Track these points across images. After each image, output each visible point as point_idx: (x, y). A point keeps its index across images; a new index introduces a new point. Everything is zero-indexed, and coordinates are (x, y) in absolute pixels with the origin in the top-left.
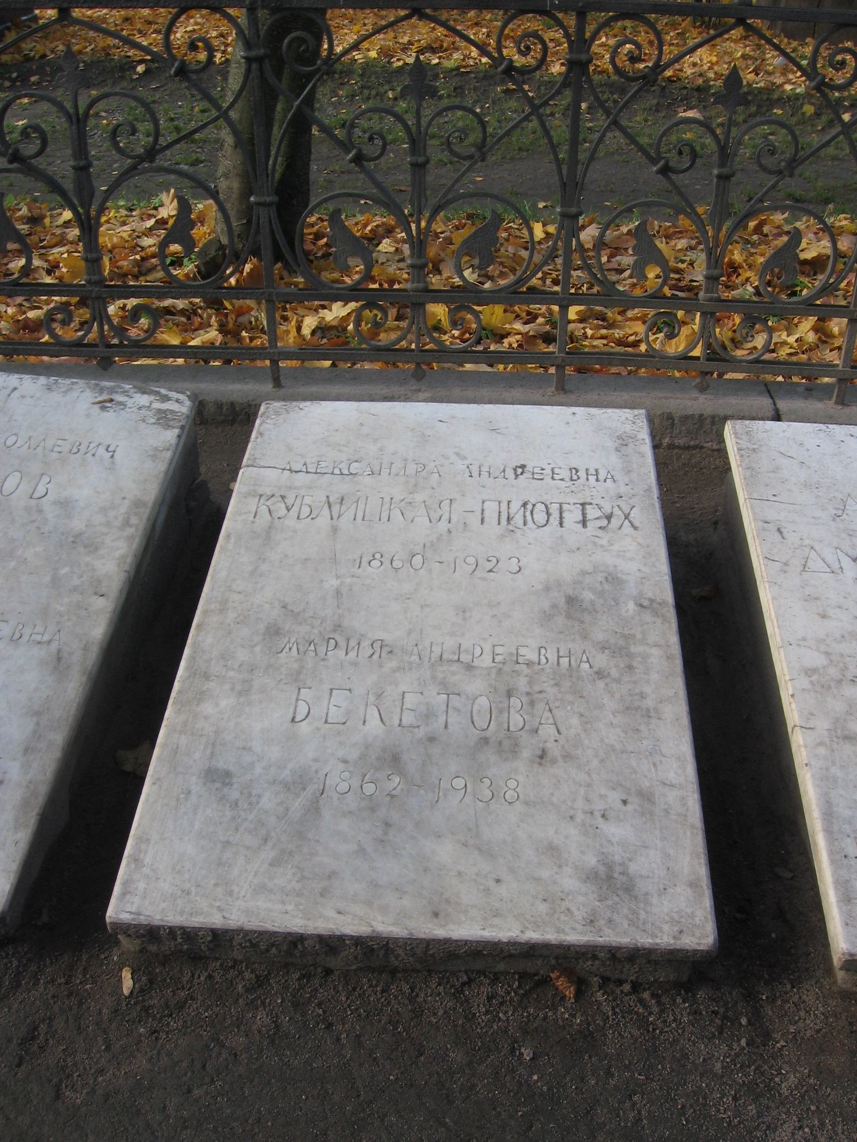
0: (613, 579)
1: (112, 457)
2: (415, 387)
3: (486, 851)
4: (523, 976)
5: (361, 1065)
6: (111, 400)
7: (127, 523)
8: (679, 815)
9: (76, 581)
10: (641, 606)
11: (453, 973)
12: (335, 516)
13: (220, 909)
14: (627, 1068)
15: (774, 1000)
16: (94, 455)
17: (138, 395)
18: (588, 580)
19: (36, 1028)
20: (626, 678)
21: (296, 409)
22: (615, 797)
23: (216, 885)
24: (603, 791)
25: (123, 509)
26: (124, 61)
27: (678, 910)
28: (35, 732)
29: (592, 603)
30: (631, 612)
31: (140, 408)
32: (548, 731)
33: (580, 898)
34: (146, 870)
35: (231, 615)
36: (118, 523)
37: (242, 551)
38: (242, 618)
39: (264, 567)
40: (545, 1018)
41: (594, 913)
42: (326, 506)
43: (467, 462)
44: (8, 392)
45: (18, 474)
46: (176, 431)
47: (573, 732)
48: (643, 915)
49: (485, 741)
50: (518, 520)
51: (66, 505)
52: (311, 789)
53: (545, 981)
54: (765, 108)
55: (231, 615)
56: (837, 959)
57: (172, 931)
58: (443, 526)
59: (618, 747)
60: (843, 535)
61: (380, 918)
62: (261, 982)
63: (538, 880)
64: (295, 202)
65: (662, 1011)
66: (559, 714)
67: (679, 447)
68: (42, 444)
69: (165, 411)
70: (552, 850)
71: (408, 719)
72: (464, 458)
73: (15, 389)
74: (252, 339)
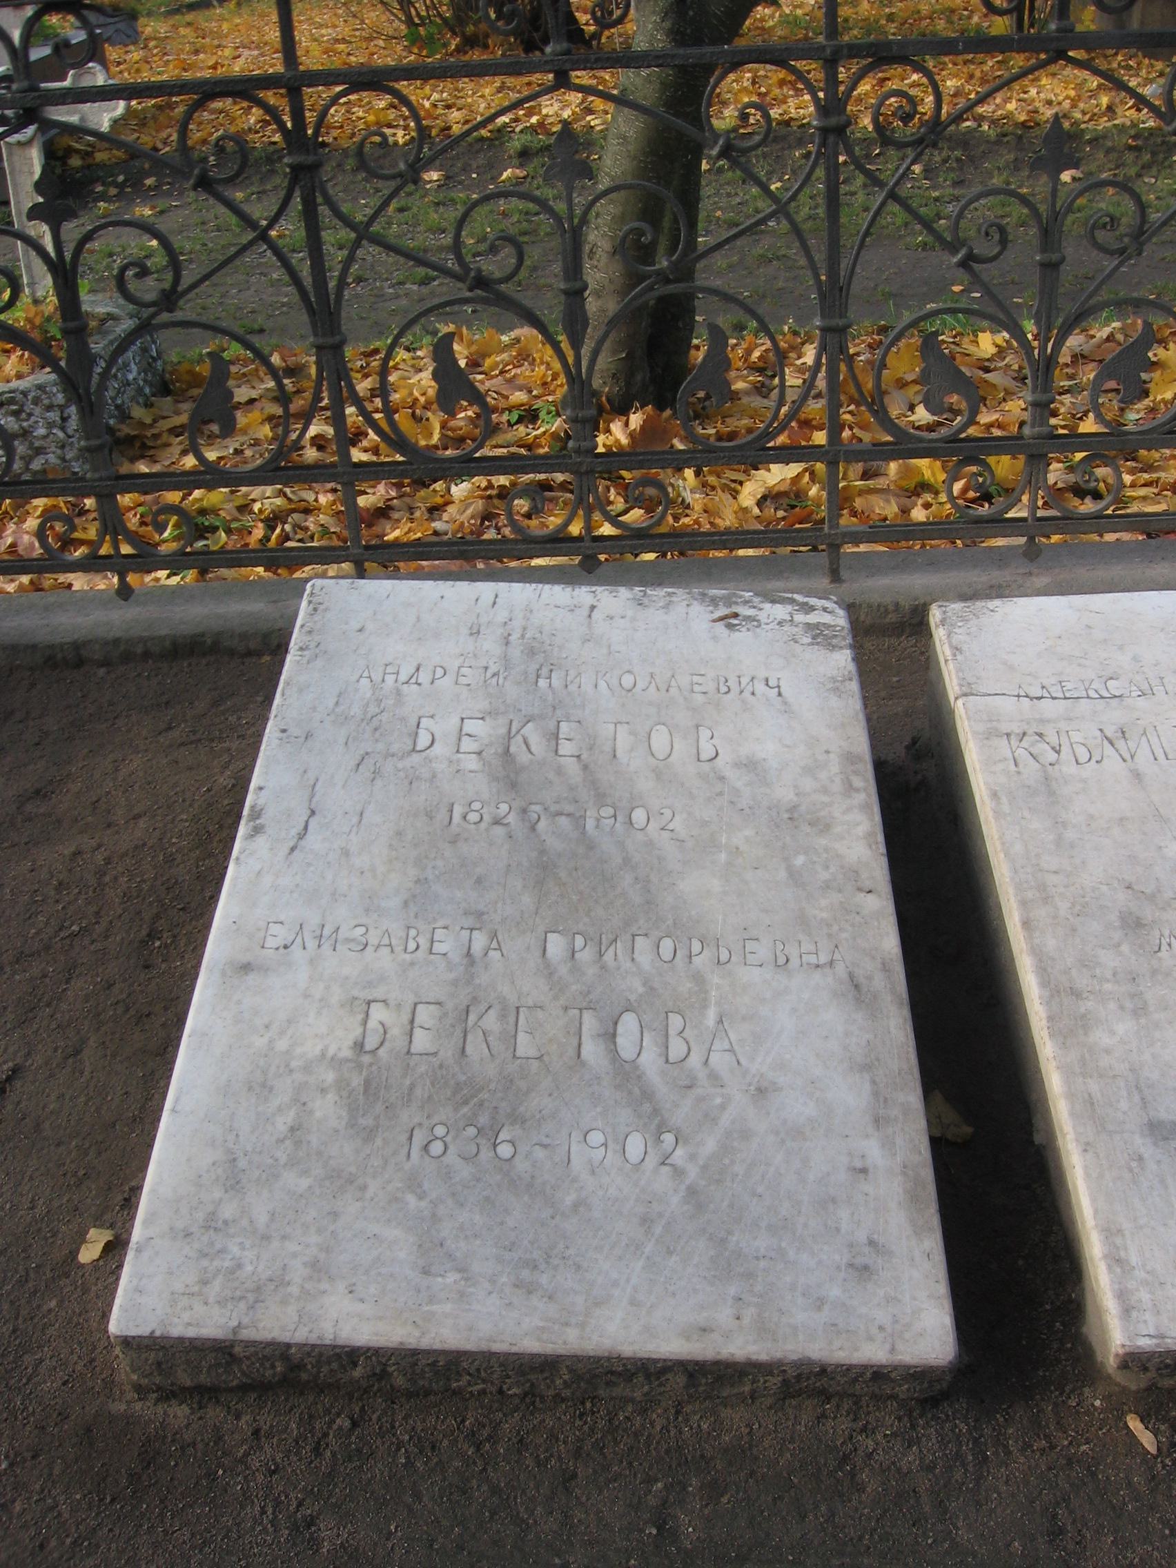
1: (780, 694)
6: (736, 615)
7: (849, 788)
9: (824, 875)
12: (1128, 757)
16: (753, 694)
17: (767, 606)
19: (1054, 1516)
21: (985, 610)
25: (835, 769)
26: (272, 148)
28: (876, 1094)
31: (780, 623)
34: (1140, 1274)
35: (1063, 907)
36: (837, 786)
37: (1026, 814)
38: (1078, 907)
42: (1105, 742)
44: (586, 613)
51: (751, 765)
54: (1161, 156)
64: (680, 324)
68: (673, 683)
69: (817, 626)
73: (593, 608)
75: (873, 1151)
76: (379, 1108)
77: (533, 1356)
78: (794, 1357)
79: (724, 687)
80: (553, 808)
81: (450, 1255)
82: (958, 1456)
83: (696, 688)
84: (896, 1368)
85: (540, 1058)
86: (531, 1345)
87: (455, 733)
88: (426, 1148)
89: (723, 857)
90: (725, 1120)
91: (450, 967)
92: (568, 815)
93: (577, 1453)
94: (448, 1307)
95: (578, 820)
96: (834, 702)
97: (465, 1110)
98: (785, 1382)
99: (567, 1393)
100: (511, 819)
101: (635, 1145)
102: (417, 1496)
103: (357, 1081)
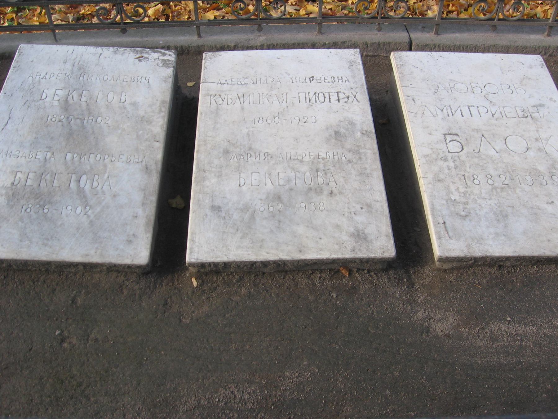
0: (351, 123)
2: (258, 35)
3: (315, 228)
4: (330, 270)
5: (280, 303)
6: (142, 57)
7: (160, 111)
8: (381, 212)
9: (146, 137)
10: (363, 133)
11: (307, 271)
12: (242, 103)
13: (226, 255)
14: (368, 297)
15: (415, 273)
17: (153, 54)
18: (342, 124)
19: (167, 301)
20: (359, 162)
22: (358, 207)
23: (223, 247)
24: (354, 205)
25: (158, 105)
27: (383, 245)
28: (144, 197)
29: (344, 133)
30: (359, 136)
31: (155, 59)
32: (332, 184)
33: (350, 243)
34: (197, 244)
35: (209, 146)
36: (157, 111)
37: (208, 119)
39: (218, 126)
40: (339, 283)
41: (354, 247)
43: (290, 76)
44: (98, 56)
45: (112, 93)
46: (172, 69)
47: (341, 183)
48: (370, 247)
49: (310, 189)
50: (313, 100)
51: (134, 104)
52: (250, 210)
53: (338, 271)
55: (209, 146)
56: (436, 258)
57: (210, 264)
58: (284, 104)
59: (358, 188)
60: (438, 100)
61: (281, 254)
62: (241, 279)
63: (334, 237)
65: (378, 279)
66: (336, 177)
67: (370, 56)
69: (165, 60)
70: (338, 227)
71: (282, 182)
72: (289, 75)
73: (101, 54)
74: (175, 6)
75: (140, 212)
76: (16, 200)
77: (44, 261)
78: (107, 262)
79: (133, 80)
80: (76, 117)
81: (27, 237)
82: (149, 287)
83: (125, 80)
84: (133, 265)
85: (59, 187)
86: (44, 258)
87: (53, 93)
88: (26, 210)
89: (120, 131)
90: (103, 204)
91: (40, 162)
92: (80, 119)
93: (57, 284)
94: (25, 249)
95: (82, 121)
96: (164, 85)
97: (37, 200)
98: (107, 268)
99: (56, 270)
100: (64, 120)
101: (79, 210)
102: (17, 294)
103: (11, 193)
